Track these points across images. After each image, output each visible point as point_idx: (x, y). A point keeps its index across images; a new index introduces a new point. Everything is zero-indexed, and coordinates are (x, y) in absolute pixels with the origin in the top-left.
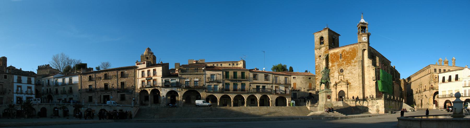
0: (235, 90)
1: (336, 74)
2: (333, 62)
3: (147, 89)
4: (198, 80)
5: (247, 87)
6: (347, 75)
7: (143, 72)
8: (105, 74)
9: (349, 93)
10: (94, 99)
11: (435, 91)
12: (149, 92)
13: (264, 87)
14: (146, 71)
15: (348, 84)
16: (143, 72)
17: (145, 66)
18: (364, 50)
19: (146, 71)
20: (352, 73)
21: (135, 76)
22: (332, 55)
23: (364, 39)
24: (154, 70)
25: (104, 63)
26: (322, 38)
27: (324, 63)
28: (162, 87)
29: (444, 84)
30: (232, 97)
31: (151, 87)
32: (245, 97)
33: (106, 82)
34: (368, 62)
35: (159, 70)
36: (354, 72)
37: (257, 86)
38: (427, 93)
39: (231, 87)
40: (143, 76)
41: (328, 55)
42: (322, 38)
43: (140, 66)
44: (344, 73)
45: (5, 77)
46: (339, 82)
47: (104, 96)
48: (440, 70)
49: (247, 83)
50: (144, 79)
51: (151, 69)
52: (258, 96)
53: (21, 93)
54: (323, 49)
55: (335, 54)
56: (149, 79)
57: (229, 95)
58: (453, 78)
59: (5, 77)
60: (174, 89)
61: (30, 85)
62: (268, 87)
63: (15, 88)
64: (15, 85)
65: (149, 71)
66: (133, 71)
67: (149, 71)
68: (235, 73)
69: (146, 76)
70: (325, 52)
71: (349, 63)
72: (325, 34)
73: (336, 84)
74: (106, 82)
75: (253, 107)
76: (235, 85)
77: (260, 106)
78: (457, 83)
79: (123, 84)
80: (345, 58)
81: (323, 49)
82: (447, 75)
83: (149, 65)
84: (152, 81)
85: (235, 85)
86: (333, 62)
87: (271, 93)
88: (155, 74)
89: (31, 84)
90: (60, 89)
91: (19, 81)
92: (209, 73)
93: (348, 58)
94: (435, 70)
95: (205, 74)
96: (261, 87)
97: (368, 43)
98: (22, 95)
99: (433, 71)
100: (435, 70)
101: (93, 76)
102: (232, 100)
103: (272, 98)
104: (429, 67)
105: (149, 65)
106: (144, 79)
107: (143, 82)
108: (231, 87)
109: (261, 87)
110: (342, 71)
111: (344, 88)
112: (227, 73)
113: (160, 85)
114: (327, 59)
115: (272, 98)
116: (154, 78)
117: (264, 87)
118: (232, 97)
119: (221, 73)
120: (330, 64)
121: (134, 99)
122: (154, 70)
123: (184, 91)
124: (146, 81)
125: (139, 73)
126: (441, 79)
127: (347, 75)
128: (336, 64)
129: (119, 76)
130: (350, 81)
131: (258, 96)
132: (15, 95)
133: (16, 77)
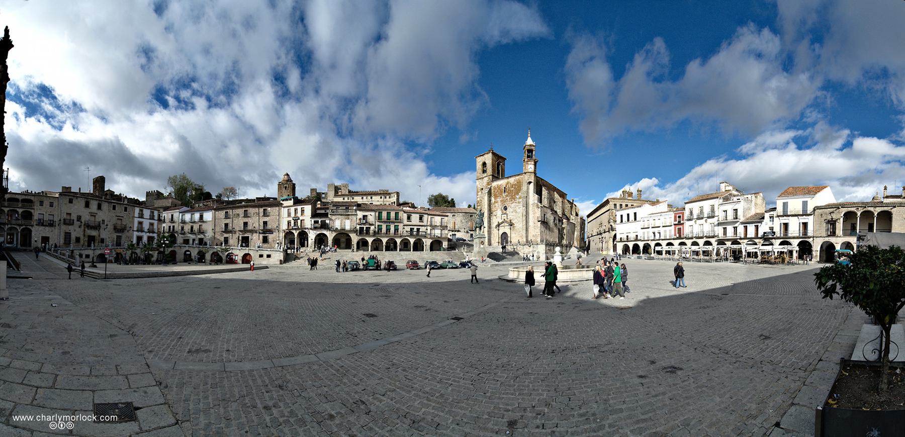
1: (499, 213)
2: (496, 197)
3: (294, 231)
6: (511, 215)
12: (296, 235)
13: (418, 230)
14: (293, 209)
15: (511, 224)
18: (530, 183)
20: (515, 212)
22: (495, 188)
23: (530, 167)
26: (484, 164)
27: (486, 198)
29: (622, 225)
30: (385, 240)
31: (298, 229)
32: (398, 241)
33: (246, 220)
34: (533, 198)
36: (518, 210)
38: (606, 235)
40: (289, 215)
41: (490, 189)
42: (484, 164)
43: (285, 203)
44: (508, 211)
48: (627, 205)
49: (401, 226)
50: (291, 219)
51: (299, 208)
52: (412, 240)
53: (142, 231)
54: (486, 179)
55: (499, 187)
58: (632, 217)
61: (152, 221)
62: (422, 229)
63: (136, 225)
64: (136, 220)
68: (389, 214)
69: (293, 215)
70: (488, 184)
71: (513, 198)
72: (488, 158)
73: (499, 225)
74: (246, 220)
78: (636, 224)
79: (265, 223)
80: (510, 192)
81: (486, 179)
82: (624, 213)
86: (496, 197)
87: (425, 237)
89: (153, 219)
90: (187, 228)
91: (141, 216)
92: (360, 214)
93: (513, 192)
94: (615, 205)
97: (535, 173)
98: (143, 234)
99: (613, 207)
100: (615, 205)
103: (427, 242)
104: (607, 202)
107: (289, 223)
110: (506, 208)
111: (507, 229)
112: (380, 214)
113: (309, 227)
114: (490, 193)
115: (427, 242)
117: (418, 230)
118: (385, 240)
119: (373, 213)
120: (493, 199)
123: (334, 234)
124: (292, 222)
126: (618, 219)
127: (511, 215)
128: (499, 200)
129: (261, 214)
131: (412, 240)
132: (136, 234)
133: (137, 210)
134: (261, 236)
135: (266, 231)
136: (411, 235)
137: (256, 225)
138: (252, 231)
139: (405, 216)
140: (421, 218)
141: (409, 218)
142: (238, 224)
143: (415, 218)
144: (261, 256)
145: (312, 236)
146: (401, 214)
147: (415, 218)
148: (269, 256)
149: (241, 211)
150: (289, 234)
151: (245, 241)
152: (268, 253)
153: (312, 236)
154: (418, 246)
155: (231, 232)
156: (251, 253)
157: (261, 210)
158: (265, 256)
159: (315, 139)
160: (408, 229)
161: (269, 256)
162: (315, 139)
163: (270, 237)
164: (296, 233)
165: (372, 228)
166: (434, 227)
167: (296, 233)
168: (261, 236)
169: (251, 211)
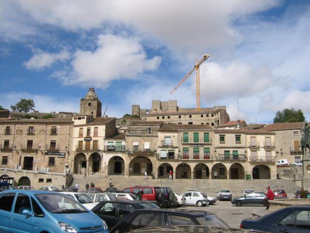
0: (196, 157)
3: (86, 154)
5: (212, 153)
8: (30, 127)
10: (10, 162)
11: (155, 171)
14: (85, 129)
17: (83, 121)
21: (70, 134)
24: (206, 134)
25: (24, 100)
28: (104, 151)
33: (30, 138)
35: (102, 129)
37: (225, 151)
39: (191, 153)
40: (81, 135)
47: (25, 158)
50: (82, 139)
51: (92, 128)
52: (228, 166)
56: (88, 139)
57: (188, 164)
60: (120, 155)
65: (89, 130)
66: (68, 127)
67: (89, 130)
69: (85, 135)
74: (30, 138)
75: (135, 176)
76: (196, 151)
77: (253, 178)
83: (90, 120)
84: (92, 142)
85: (196, 151)
87: (244, 161)
88: (96, 134)
95: (157, 136)
96: (231, 153)
102: (192, 170)
103: (248, 168)
105: (90, 120)
107: (80, 142)
108: (191, 153)
109: (231, 153)
115: (248, 168)
116: (94, 139)
121: (67, 164)
122: (206, 134)
124: (84, 143)
125: (76, 131)
129: (49, 132)
131: (228, 166)
134: (47, 157)
135: (53, 150)
136: (227, 159)
137: (42, 144)
138: (36, 151)
139: (217, 136)
140: (238, 138)
141: (222, 139)
142: (23, 140)
143: (230, 139)
144: (41, 180)
145: (106, 158)
146: (211, 134)
147: (230, 139)
148: (49, 180)
149: (25, 128)
150: (80, 155)
151: (28, 164)
152: (49, 177)
153: (106, 158)
154: (237, 173)
155: (11, 151)
156: (31, 177)
157: (50, 127)
158: (45, 181)
159: (259, 158)
160: (222, 152)
161: (49, 180)
162: (259, 158)
163: (58, 160)
164: (88, 156)
165: (176, 151)
166: (254, 148)
167: (88, 156)
168: (47, 157)
169: (37, 128)
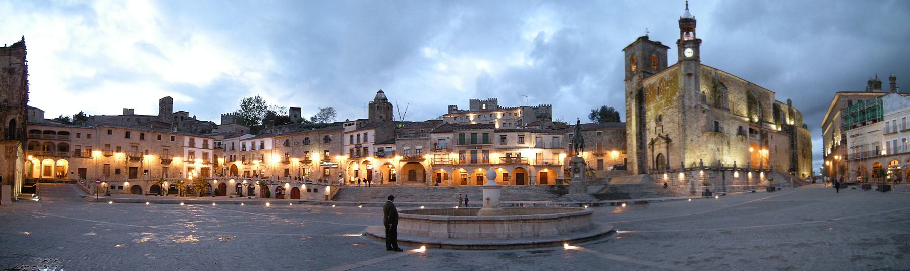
4: (408, 148)
7: (352, 137)
9: (671, 158)
14: (355, 137)
16: (352, 137)
19: (355, 137)
21: (342, 143)
45: (173, 139)
46: (657, 139)
51: (362, 133)
59: (173, 139)
65: (359, 135)
67: (359, 135)
69: (355, 142)
73: (653, 143)
88: (365, 140)
95: (430, 139)
101: (468, 134)
106: (364, 145)
125: (347, 138)
130: (671, 137)
